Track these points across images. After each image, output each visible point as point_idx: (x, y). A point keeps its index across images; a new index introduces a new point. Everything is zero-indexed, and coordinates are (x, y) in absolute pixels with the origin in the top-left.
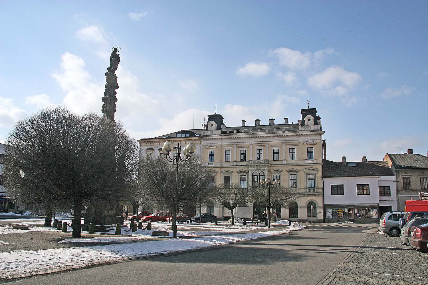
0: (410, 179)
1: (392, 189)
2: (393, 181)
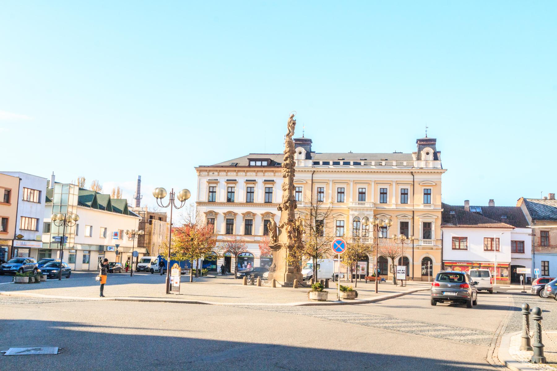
0: (550, 232)
1: (469, 240)
2: (529, 235)
